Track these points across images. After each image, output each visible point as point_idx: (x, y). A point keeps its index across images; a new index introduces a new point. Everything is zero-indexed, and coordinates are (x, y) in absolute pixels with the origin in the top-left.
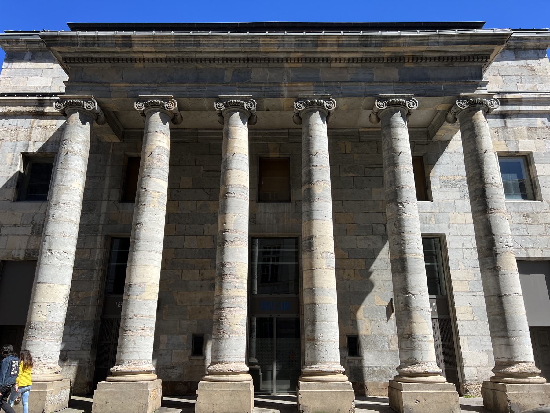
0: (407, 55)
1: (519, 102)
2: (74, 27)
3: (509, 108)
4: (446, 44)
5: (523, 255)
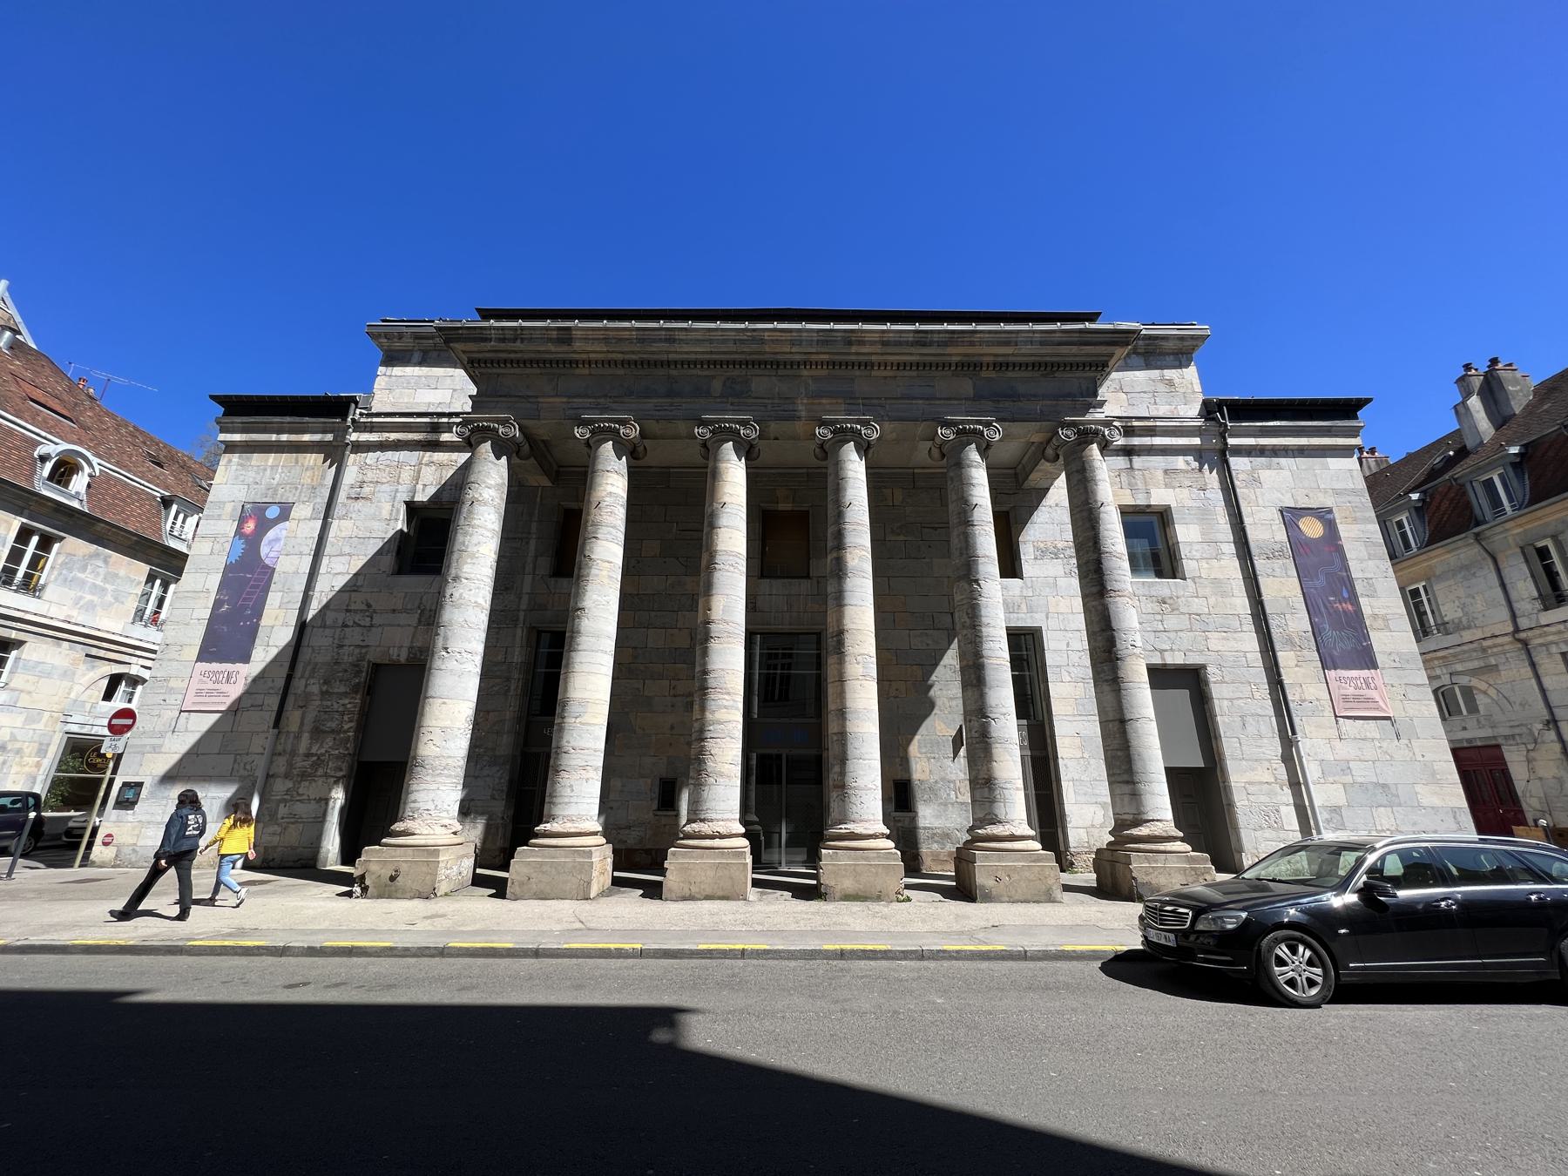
0: (986, 359)
1: (1151, 431)
2: (486, 314)
3: (1136, 441)
4: (1042, 343)
5: (1157, 660)
